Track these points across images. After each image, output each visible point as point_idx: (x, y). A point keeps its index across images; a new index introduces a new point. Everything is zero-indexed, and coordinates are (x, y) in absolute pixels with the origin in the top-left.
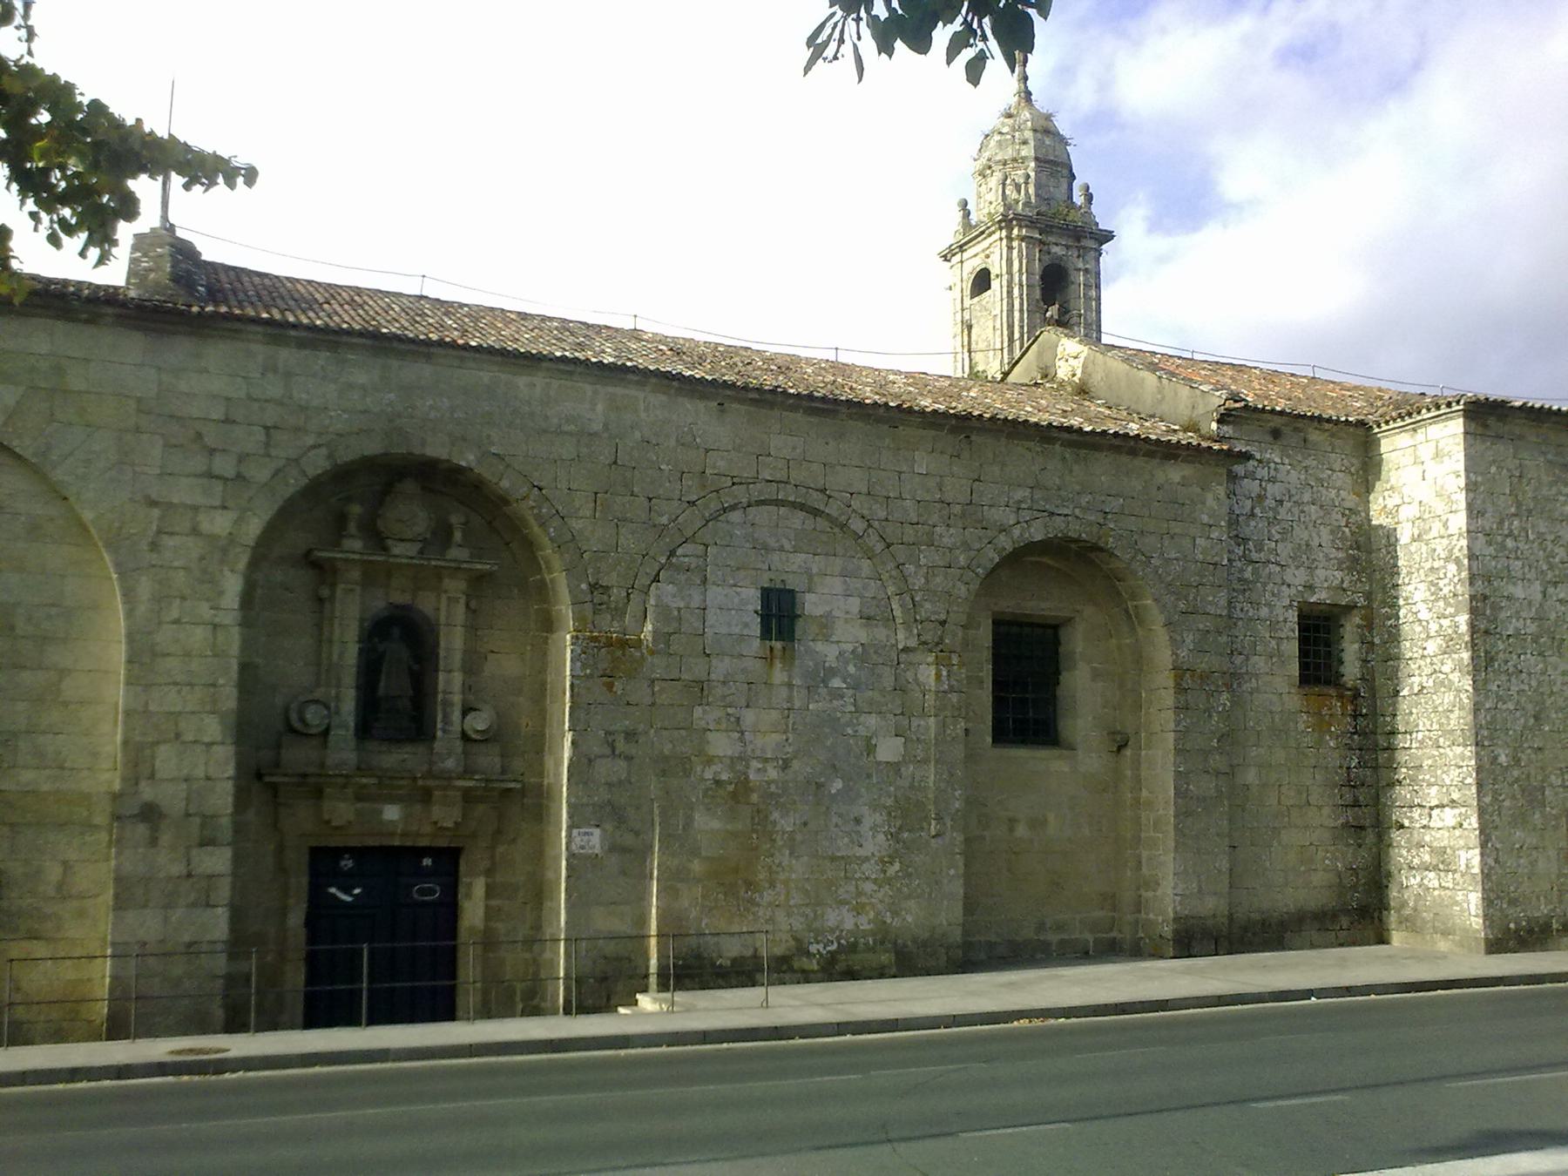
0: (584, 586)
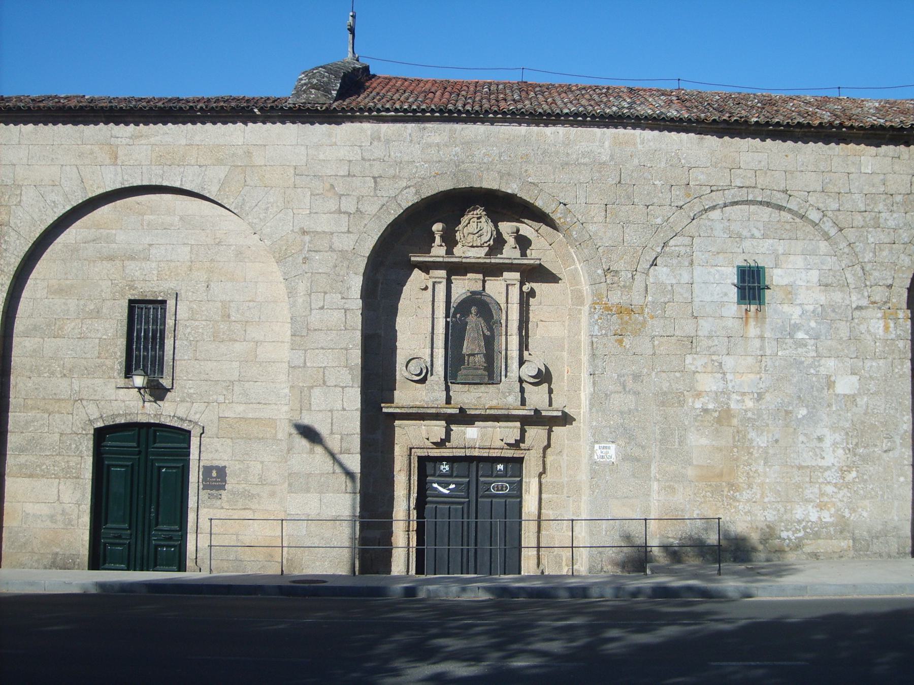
0: (600, 271)
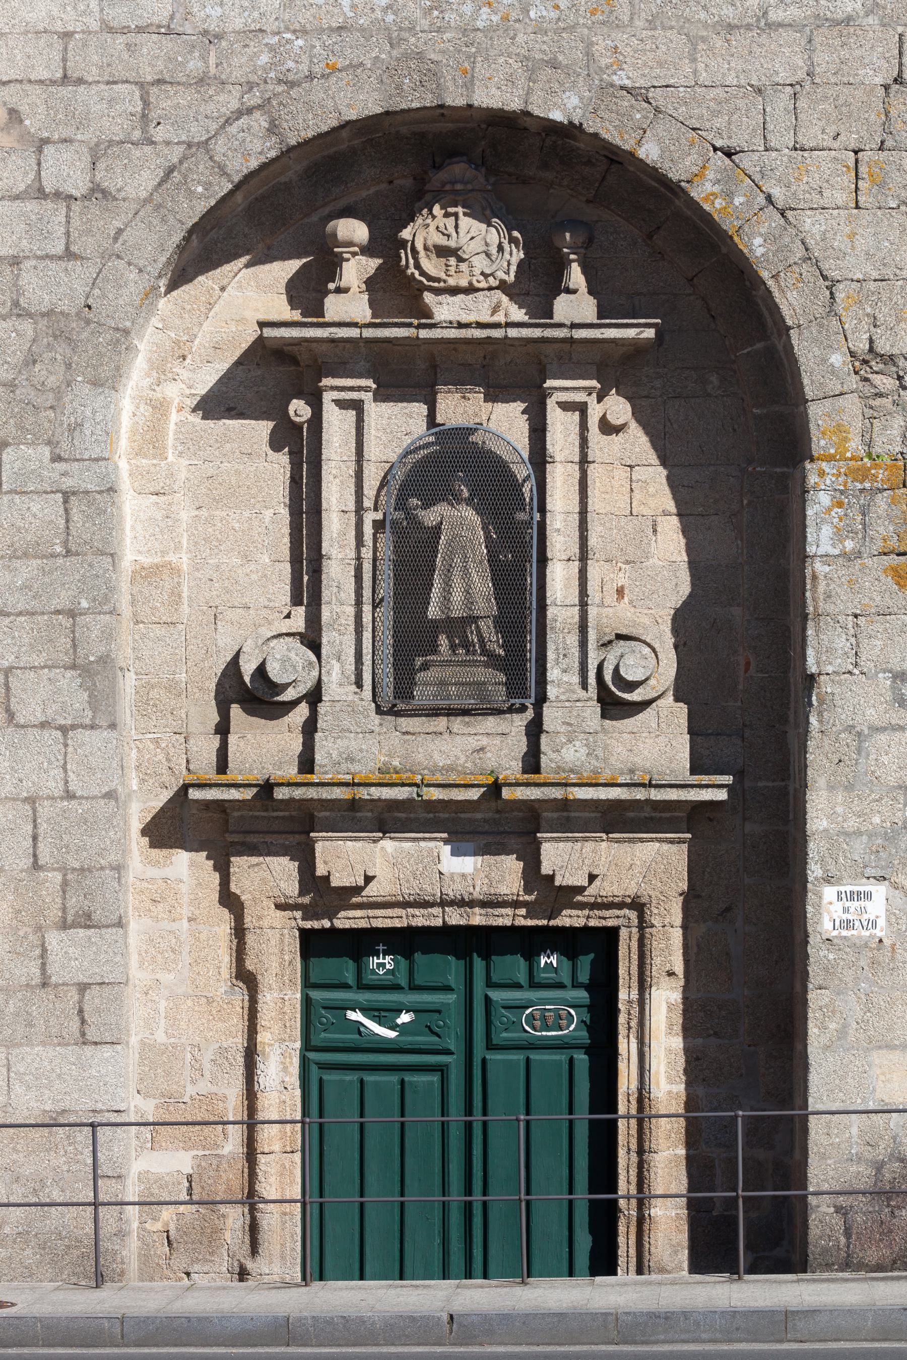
0: (837, 359)
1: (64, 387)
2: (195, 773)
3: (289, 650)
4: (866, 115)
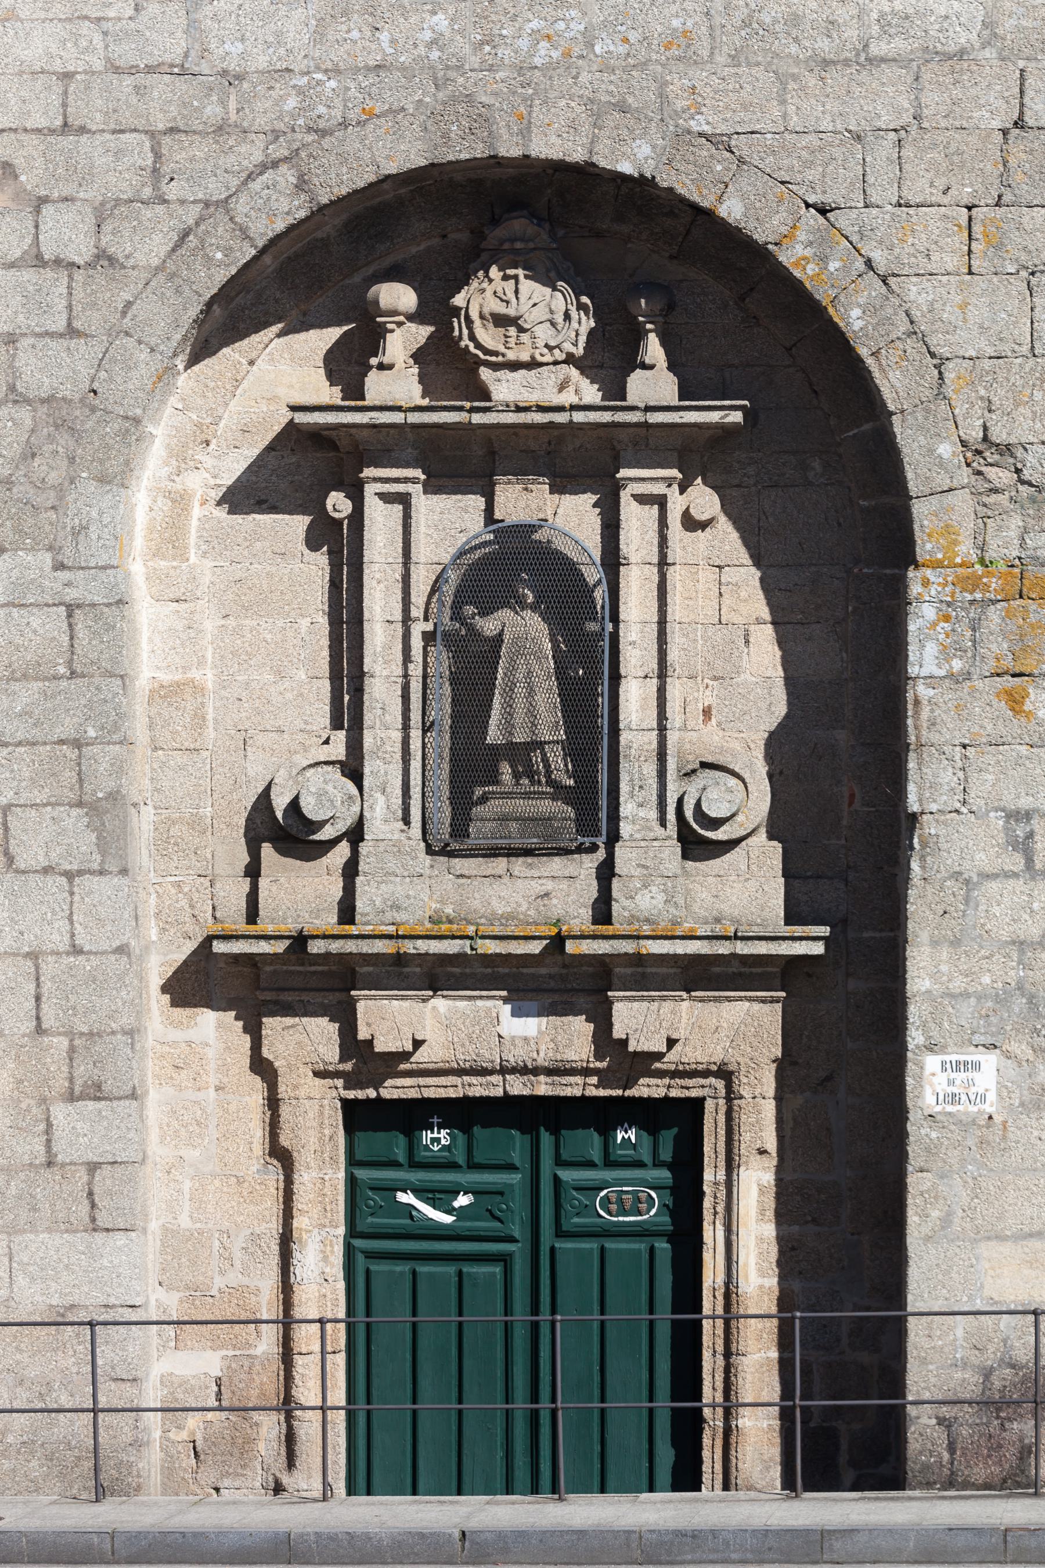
0: (946, 450)
1: (66, 484)
2: (222, 922)
3: (325, 782)
4: (981, 165)
